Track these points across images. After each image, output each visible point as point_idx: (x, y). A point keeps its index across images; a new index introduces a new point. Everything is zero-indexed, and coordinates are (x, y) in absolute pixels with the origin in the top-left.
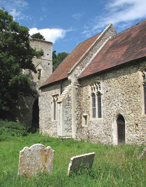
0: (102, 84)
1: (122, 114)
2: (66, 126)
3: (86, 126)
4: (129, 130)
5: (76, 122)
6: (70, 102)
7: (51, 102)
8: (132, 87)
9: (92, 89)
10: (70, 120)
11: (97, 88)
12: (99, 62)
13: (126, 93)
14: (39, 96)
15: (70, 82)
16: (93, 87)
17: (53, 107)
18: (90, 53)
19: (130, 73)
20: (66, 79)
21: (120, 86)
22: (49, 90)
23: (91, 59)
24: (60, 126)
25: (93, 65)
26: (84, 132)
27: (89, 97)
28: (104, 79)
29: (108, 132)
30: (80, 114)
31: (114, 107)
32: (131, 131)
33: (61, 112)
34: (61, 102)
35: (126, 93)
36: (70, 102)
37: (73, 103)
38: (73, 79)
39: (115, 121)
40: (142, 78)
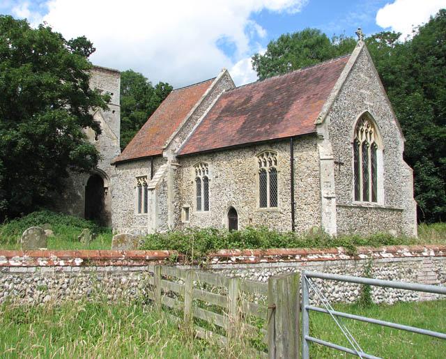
1: (234, 206)
2: (160, 222)
9: (260, 163)
10: (166, 213)
12: (207, 134)
13: (240, 181)
14: (264, 229)
17: (138, 195)
20: (160, 156)
25: (197, 136)
27: (192, 182)
30: (179, 205)
31: (224, 197)
33: (154, 203)
35: (240, 181)
36: (166, 189)
37: (169, 190)
38: (169, 156)
39: (226, 215)
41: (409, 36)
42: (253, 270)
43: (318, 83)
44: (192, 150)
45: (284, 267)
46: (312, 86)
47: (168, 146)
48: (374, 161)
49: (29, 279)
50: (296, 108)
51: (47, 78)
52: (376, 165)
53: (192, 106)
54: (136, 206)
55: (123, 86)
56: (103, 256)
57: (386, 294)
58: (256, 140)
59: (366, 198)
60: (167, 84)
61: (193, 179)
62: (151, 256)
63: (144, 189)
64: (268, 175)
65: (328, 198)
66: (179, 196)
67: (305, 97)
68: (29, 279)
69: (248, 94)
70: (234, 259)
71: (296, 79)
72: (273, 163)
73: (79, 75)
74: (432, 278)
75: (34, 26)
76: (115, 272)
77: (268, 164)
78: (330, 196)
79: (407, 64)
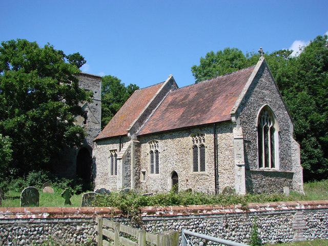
1: (176, 171)
8: (185, 148)
9: (193, 141)
10: (129, 176)
11: (155, 147)
19: (183, 137)
20: (126, 135)
28: (161, 139)
31: (169, 165)
36: (129, 158)
41: (297, 52)
42: (172, 221)
43: (233, 86)
45: (195, 219)
46: (230, 88)
48: (272, 140)
49: (10, 229)
50: (217, 103)
51: (49, 80)
52: (274, 142)
53: (148, 101)
54: (109, 170)
55: (104, 87)
56: (63, 211)
57: (270, 237)
58: (190, 125)
59: (267, 165)
60: (135, 85)
61: (148, 152)
62: (98, 211)
64: (199, 149)
66: (138, 163)
67: (224, 95)
68: (10, 229)
70: (158, 213)
71: (219, 83)
72: (202, 141)
73: (71, 78)
74: (303, 225)
75: (41, 46)
76: (72, 223)
78: (241, 164)
79: (297, 71)
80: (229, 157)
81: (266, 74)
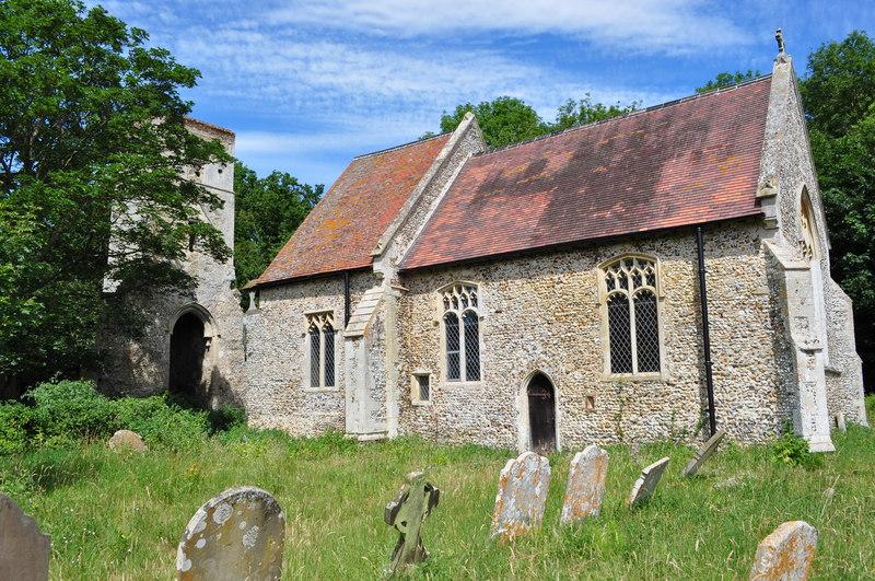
0: (482, 291)
1: (546, 371)
2: (374, 406)
3: (425, 403)
4: (568, 412)
5: (398, 392)
6: (382, 336)
7: (300, 333)
8: (578, 305)
15: (379, 280)
16: (449, 297)
18: (427, 197)
19: (571, 271)
20: (369, 269)
21: (539, 300)
22: (293, 297)
23: (428, 216)
24: (355, 404)
26: (421, 419)
27: (437, 324)
28: (487, 278)
29: (501, 418)
31: (520, 353)
32: (573, 415)
33: (361, 365)
34: (362, 336)
36: (382, 336)
40: (605, 285)
44: (436, 259)
47: (385, 251)
63: (323, 339)
65: (810, 352)
69: (533, 157)
77: (460, 304)
80: (754, 325)
81: (273, 274)
